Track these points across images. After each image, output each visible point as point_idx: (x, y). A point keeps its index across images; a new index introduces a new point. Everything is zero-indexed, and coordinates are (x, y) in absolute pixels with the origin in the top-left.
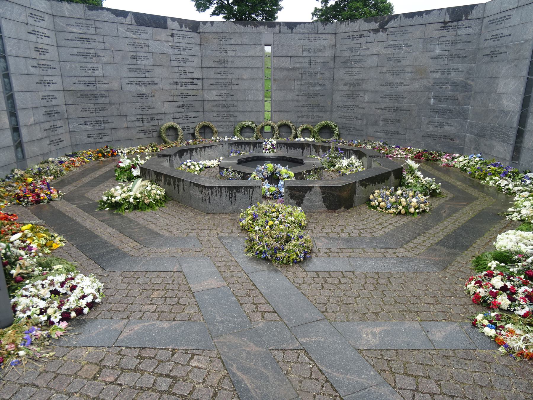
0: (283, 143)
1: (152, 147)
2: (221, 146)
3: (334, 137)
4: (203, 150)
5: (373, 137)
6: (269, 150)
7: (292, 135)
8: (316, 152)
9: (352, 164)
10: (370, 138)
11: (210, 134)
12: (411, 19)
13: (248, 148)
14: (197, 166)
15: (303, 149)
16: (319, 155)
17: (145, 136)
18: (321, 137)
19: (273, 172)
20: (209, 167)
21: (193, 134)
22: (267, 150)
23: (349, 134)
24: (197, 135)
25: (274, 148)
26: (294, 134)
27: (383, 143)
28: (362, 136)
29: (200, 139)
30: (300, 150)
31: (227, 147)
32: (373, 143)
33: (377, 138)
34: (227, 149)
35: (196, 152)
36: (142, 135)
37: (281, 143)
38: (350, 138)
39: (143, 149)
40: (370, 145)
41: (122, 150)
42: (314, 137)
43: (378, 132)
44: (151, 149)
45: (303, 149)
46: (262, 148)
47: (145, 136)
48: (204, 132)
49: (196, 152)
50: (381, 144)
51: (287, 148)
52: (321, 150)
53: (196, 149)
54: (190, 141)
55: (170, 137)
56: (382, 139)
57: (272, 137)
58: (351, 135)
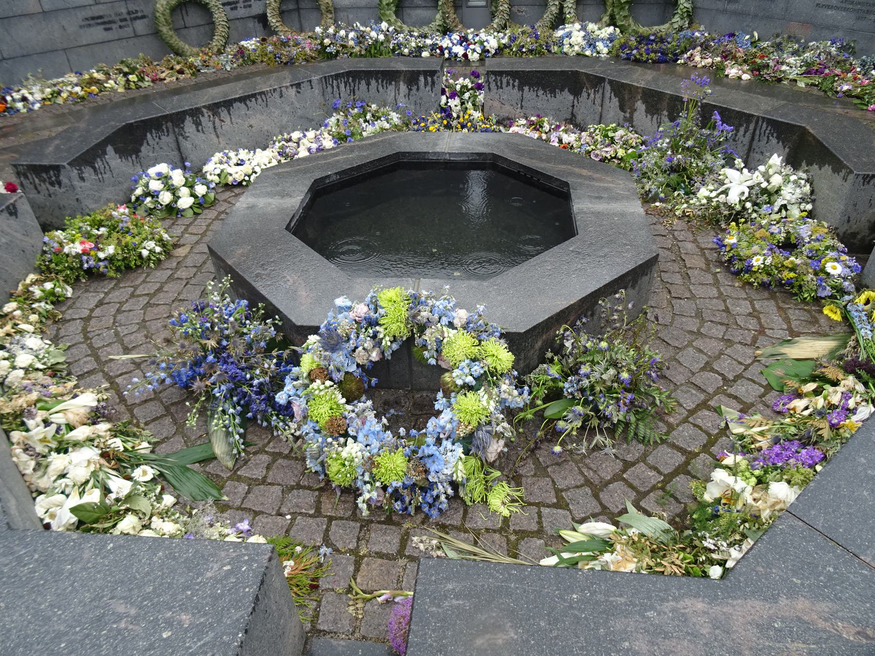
0: (508, 73)
1: (126, 74)
2: (292, 92)
3: (677, 18)
4: (224, 113)
5: (808, 23)
6: (462, 93)
7: (548, 17)
8: (622, 108)
9: (771, 194)
10: (796, 29)
11: (314, 15)
12: (246, 151)
13: (392, 88)
14: (185, 191)
15: (576, 93)
16: (630, 120)
17: (109, 35)
18: (636, 21)
19: (411, 339)
20: (240, 184)
21: (262, 19)
22: (453, 96)
23: (724, 11)
24: (273, 20)
25: (479, 87)
26: (554, 10)
27: (841, 49)
28: (770, 18)
29: (284, 33)
30: (566, 97)
31: (317, 91)
32: (805, 48)
33: (821, 29)
34: (320, 99)
35: (198, 124)
36: (97, 33)
37: (500, 73)
38: (725, 23)
39: (97, 82)
40: (795, 53)
41: (24, 92)
42: (612, 22)
43: (829, 7)
44: (121, 79)
45: (576, 93)
46: (437, 89)
47: (109, 35)
48: (298, 9)
49: (198, 124)
50: (833, 50)
51: (521, 89)
52: (640, 106)
53: (195, 113)
54: (250, 44)
55: (193, 31)
56: (839, 34)
57: (486, 25)
58: (735, 13)
